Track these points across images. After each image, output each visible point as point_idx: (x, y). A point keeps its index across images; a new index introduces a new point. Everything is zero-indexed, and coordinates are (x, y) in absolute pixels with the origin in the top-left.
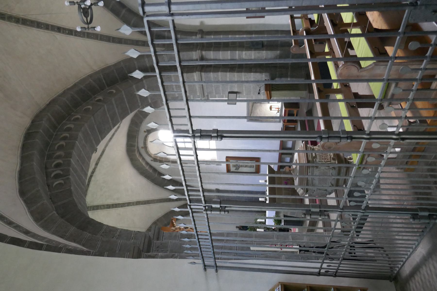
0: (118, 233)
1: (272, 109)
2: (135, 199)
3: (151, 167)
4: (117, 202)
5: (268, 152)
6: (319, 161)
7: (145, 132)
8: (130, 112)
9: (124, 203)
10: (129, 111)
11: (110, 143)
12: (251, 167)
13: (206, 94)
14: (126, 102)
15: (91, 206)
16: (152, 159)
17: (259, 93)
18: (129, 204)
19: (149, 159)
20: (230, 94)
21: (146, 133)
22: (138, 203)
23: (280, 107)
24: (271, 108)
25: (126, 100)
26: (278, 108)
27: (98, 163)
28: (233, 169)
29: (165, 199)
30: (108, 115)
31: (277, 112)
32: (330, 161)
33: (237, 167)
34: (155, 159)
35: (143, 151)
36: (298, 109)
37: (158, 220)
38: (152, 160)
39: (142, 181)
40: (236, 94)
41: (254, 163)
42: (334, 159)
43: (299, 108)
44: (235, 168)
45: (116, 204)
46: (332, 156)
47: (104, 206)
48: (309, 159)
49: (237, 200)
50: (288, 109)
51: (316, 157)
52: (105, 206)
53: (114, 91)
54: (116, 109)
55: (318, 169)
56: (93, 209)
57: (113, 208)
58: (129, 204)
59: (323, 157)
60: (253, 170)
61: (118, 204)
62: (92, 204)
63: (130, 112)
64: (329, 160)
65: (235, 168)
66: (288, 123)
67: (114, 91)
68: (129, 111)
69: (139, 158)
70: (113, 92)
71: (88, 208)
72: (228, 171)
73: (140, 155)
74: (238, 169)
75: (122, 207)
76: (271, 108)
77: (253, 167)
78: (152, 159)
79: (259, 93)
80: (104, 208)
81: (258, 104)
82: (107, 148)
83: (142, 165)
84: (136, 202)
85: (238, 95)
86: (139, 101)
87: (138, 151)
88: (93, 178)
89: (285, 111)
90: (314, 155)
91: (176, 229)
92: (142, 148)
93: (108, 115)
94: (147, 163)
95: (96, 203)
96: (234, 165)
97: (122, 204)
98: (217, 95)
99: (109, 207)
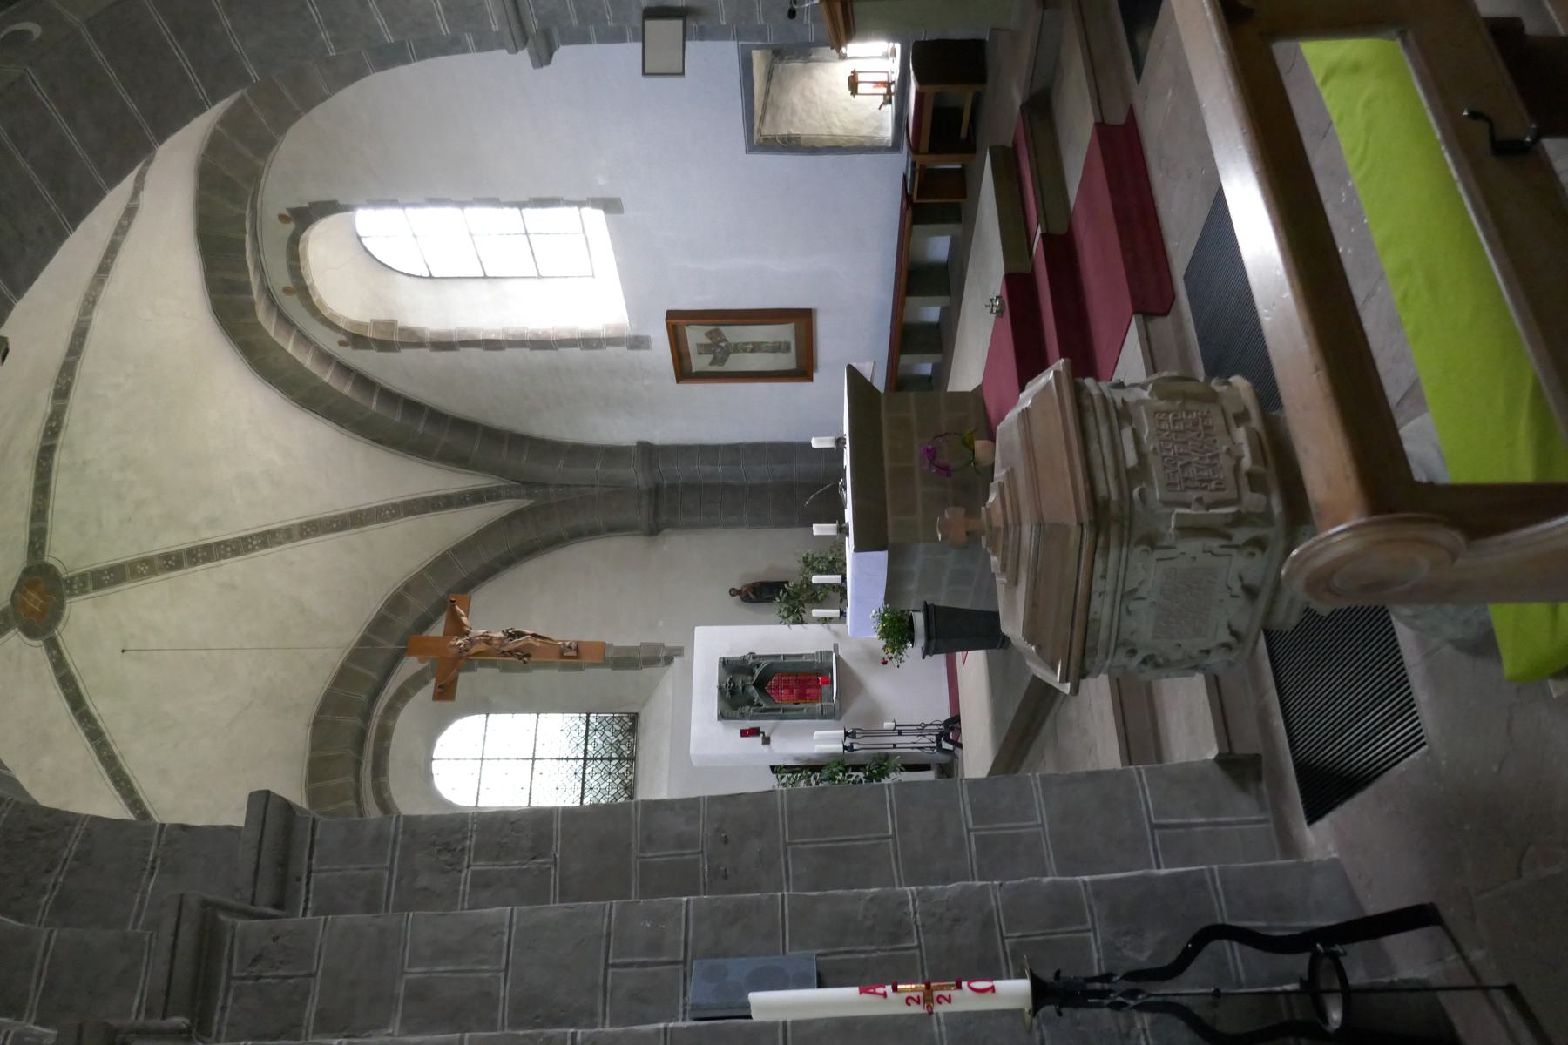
0: (74, 845)
1: (861, 88)
2: (293, 515)
3: (345, 370)
4: (210, 536)
5: (846, 280)
6: (1166, 503)
7: (283, 218)
8: (152, 138)
9: (244, 539)
10: (148, 131)
11: (111, 290)
12: (777, 348)
13: (533, 25)
14: (121, 89)
15: (83, 575)
16: (344, 338)
17: (792, 14)
18: (268, 538)
19: (329, 341)
20: (649, 23)
21: (291, 226)
22: (311, 528)
23: (895, 77)
24: (853, 84)
25: (112, 74)
26: (888, 84)
27: (69, 386)
28: (699, 363)
29: (425, 500)
30: (25, 165)
31: (881, 99)
32: (1237, 501)
33: (720, 350)
34: (357, 339)
35: (292, 305)
36: (978, 88)
37: (407, 587)
38: (342, 344)
39: (308, 434)
40: (679, 23)
41: (784, 332)
42: (1256, 482)
43: (981, 78)
44: (709, 358)
45: (207, 547)
46: (1247, 463)
47: (147, 561)
48: (1102, 490)
49: (730, 481)
50: (931, 89)
51: (1140, 473)
52: (157, 563)
53: (36, 30)
54: (66, 129)
55: (1158, 554)
56: (99, 585)
57: (195, 564)
58: (268, 538)
59: (1191, 472)
60: (787, 361)
61: (218, 544)
62: (84, 566)
63: (152, 138)
64: (1230, 493)
65: (709, 358)
66: (932, 157)
67: (36, 30)
68: (148, 131)
69: (280, 341)
70: (25, 34)
71: (70, 583)
72: (684, 373)
73: (285, 320)
74: (723, 361)
75: (236, 553)
76: (853, 84)
77: (788, 349)
78: (344, 338)
79: (792, 14)
80: (153, 572)
81: (797, 65)
82: (98, 317)
83: (299, 365)
84: (301, 525)
85: (692, 24)
86: (193, 77)
87: (272, 303)
88: (60, 458)
89: (919, 96)
90: (1131, 459)
91: (472, 642)
92: (287, 290)
93: (25, 165)
94: (325, 358)
95: (105, 557)
96: (702, 342)
97: (235, 541)
98: (592, 29)
99: (173, 561)
